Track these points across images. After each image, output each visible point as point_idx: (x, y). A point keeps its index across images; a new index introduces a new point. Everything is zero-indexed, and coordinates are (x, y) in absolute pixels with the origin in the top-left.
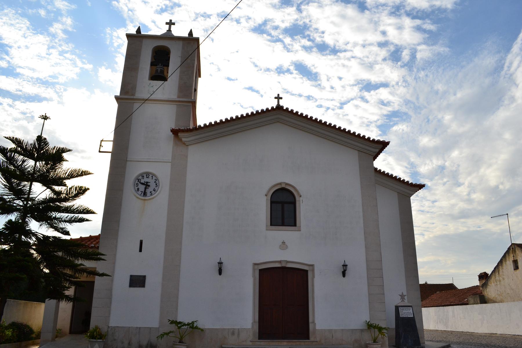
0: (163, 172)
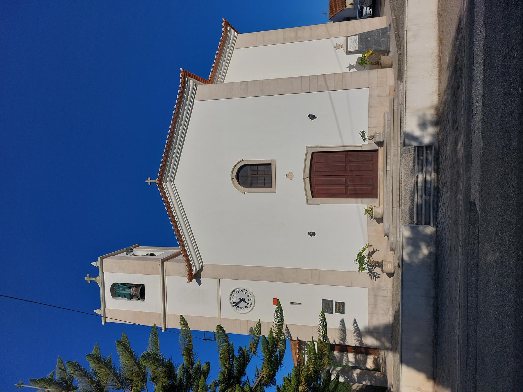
0: (229, 286)
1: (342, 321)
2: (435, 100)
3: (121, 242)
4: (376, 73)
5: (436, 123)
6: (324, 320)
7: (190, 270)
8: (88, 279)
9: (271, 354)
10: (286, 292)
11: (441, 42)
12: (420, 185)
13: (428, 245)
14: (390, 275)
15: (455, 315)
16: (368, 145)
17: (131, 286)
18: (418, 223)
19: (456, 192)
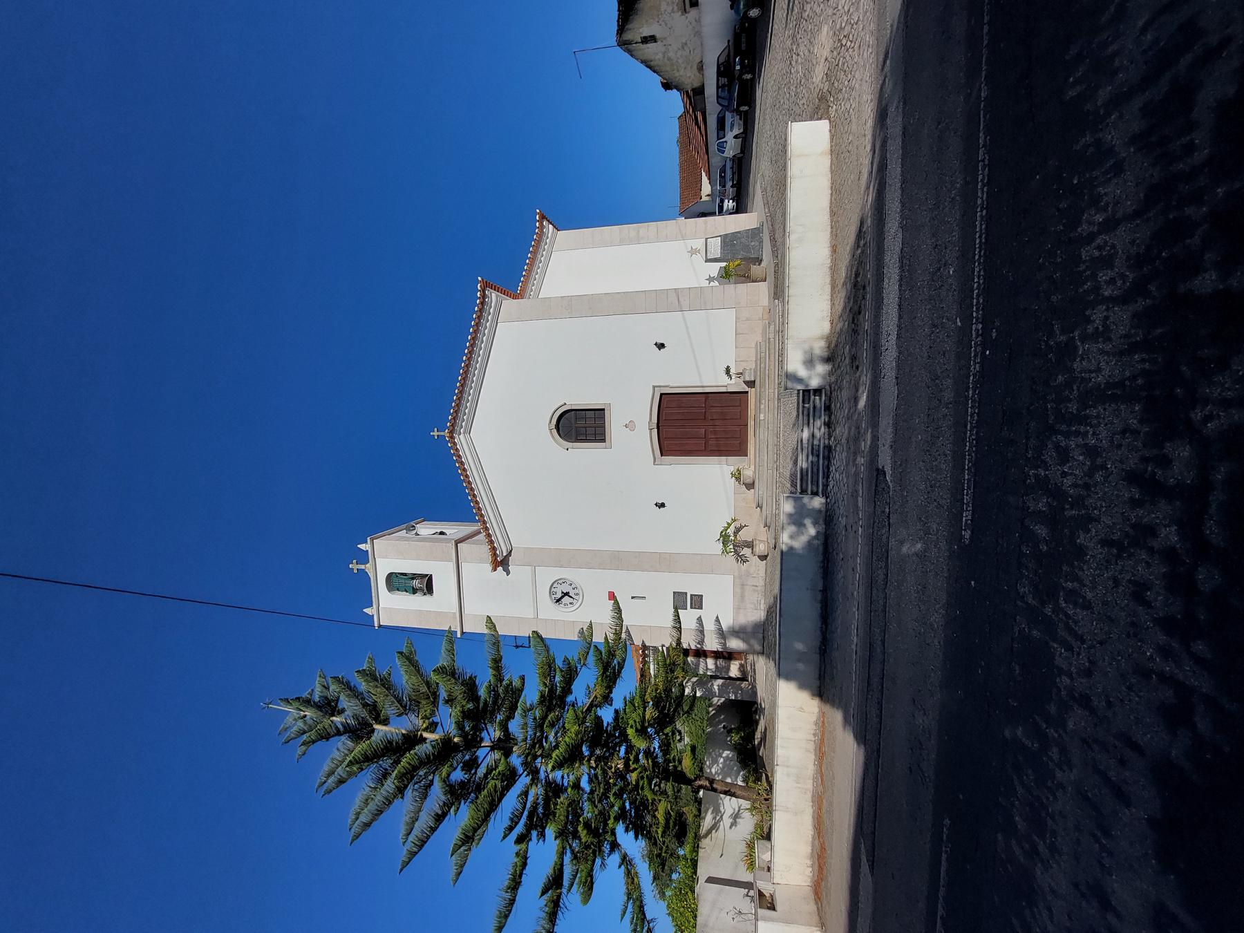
0: (547, 576)
1: (700, 619)
2: (825, 327)
3: (399, 515)
4: (743, 288)
5: (828, 360)
6: (677, 619)
7: (495, 555)
8: (354, 566)
9: (606, 666)
10: (625, 583)
11: (834, 249)
12: (805, 441)
13: (815, 523)
14: (763, 558)
15: (852, 615)
16: (735, 385)
17: (414, 577)
18: (803, 491)
19: (855, 454)
